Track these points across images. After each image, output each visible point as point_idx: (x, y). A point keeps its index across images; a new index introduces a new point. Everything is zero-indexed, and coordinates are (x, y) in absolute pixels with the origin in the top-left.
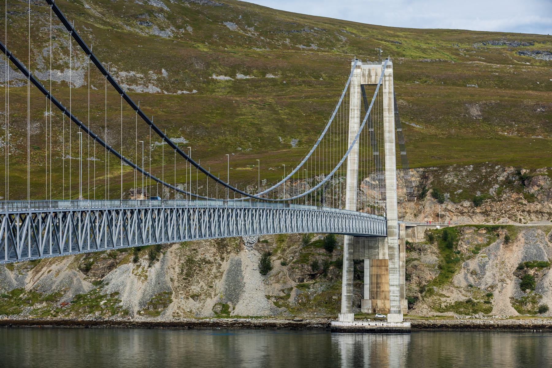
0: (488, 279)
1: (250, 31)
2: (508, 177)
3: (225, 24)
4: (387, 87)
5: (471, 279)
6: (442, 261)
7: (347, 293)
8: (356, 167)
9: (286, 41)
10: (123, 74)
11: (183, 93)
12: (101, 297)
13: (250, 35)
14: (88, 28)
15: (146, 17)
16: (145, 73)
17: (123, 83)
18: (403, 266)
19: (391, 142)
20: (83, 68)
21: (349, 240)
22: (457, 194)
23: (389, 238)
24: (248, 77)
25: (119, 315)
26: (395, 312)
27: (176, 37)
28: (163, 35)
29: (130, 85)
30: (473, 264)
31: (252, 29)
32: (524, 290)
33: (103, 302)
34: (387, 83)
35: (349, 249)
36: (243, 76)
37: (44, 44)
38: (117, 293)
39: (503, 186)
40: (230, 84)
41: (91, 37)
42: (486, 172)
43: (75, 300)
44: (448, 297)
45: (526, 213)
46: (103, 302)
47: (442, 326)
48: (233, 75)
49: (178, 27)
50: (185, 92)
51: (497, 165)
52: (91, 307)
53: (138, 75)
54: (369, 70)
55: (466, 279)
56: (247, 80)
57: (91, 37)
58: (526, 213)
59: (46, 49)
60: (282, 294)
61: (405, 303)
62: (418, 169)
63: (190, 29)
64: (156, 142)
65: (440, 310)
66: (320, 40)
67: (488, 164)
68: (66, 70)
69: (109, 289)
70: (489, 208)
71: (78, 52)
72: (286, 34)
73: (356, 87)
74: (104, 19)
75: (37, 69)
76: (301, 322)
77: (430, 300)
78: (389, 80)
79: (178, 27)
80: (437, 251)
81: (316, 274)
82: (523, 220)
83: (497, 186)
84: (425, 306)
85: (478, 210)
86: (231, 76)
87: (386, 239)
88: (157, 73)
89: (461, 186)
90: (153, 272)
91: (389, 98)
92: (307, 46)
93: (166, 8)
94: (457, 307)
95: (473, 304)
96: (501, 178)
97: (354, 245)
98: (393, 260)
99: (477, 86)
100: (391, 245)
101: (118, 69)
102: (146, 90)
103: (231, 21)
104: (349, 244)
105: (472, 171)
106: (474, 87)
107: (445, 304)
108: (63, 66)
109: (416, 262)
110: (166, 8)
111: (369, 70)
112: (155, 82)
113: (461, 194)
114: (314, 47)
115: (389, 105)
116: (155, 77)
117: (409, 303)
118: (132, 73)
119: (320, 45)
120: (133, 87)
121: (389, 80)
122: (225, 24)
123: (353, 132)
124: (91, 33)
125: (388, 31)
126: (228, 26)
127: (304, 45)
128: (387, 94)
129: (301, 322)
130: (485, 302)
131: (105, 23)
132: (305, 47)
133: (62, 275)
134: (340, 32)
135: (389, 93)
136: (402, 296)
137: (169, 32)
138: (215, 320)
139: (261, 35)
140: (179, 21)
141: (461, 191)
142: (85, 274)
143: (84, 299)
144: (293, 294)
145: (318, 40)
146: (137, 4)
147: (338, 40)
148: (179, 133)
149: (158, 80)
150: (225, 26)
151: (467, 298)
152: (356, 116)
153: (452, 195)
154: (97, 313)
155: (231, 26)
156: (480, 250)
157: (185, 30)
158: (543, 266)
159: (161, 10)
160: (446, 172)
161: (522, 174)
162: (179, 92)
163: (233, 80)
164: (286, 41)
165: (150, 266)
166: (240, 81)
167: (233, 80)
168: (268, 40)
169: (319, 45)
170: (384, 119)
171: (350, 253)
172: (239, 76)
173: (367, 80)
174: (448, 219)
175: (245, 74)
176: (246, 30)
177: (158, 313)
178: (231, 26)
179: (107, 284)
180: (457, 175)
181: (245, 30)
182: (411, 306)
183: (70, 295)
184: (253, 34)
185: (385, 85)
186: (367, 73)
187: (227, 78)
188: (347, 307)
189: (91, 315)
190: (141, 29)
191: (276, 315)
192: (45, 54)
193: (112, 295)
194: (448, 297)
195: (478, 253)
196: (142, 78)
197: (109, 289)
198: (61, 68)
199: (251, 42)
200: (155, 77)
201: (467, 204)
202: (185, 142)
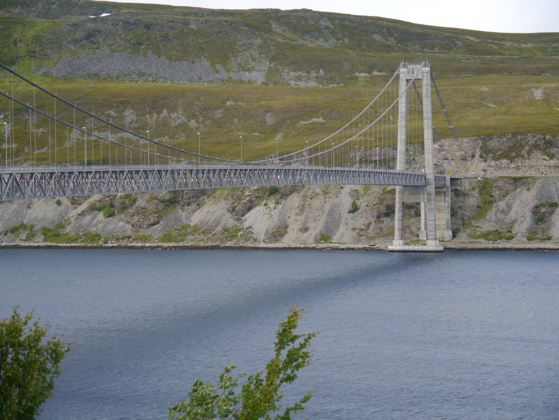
0: (512, 215)
1: (390, 40)
2: (536, 141)
3: (373, 35)
4: (425, 80)
5: (500, 216)
6: (480, 202)
7: (399, 226)
8: (404, 137)
9: (416, 46)
10: (292, 74)
11: (333, 87)
12: (240, 230)
13: (390, 43)
14: (271, 42)
15: (316, 34)
16: (309, 73)
17: (291, 80)
18: (448, 207)
19: (428, 119)
20: (265, 71)
21: (400, 189)
22: (498, 155)
23: (427, 187)
24: (381, 74)
25: (250, 242)
26: (432, 239)
27: (335, 47)
28: (326, 45)
29: (296, 82)
30: (502, 205)
31: (392, 39)
32: (537, 223)
33: (241, 233)
34: (425, 78)
35: (399, 195)
36: (377, 73)
37: (239, 54)
38: (250, 227)
39: (532, 148)
40: (368, 79)
41: (272, 48)
42: (521, 139)
43: (222, 232)
44: (482, 228)
45: (546, 167)
46: (241, 233)
47: (273, 248)
48: (370, 72)
49: (338, 40)
50: (334, 85)
51: (529, 133)
52: (232, 237)
53: (303, 74)
54: (413, 69)
55: (496, 215)
56: (380, 76)
57: (272, 48)
58: (546, 167)
59: (240, 57)
60: (363, 227)
61: (450, 233)
62: (471, 138)
63: (346, 40)
64: (302, 122)
65: (473, 237)
66: (442, 45)
67: (523, 132)
68: (252, 71)
69: (246, 224)
70: (520, 164)
71: (262, 59)
72: (417, 42)
73: (404, 82)
74: (285, 35)
75: (233, 72)
76: (373, 247)
77: (468, 231)
78: (427, 76)
79: (338, 40)
80: (477, 195)
81: (389, 213)
82: (544, 172)
83: (527, 148)
84: (464, 235)
85: (512, 165)
86: (369, 73)
87: (425, 188)
88: (316, 73)
89: (501, 149)
90: (276, 213)
91: (427, 89)
92: (431, 49)
93: (331, 26)
94: (486, 236)
95: (500, 233)
96: (531, 142)
97: (402, 192)
98: (430, 203)
99: (550, 75)
100: (429, 192)
101: (289, 70)
102: (307, 85)
103: (378, 33)
104: (400, 192)
105: (510, 138)
106: (548, 75)
107: (479, 232)
108: (251, 69)
109: (461, 204)
110: (331, 26)
111: (413, 69)
112: (314, 79)
113: (500, 155)
114: (436, 50)
115: (427, 93)
116: (314, 75)
117: (453, 233)
118: (299, 73)
119: (441, 48)
120: (298, 83)
121: (427, 76)
122: (373, 35)
123: (402, 113)
124: (273, 45)
125: (467, 37)
126: (375, 37)
127: (429, 49)
128: (425, 86)
129: (373, 247)
130: (508, 232)
131: (285, 38)
132: (429, 51)
133: (216, 215)
134: (458, 39)
135: (427, 85)
136: (448, 228)
137: (330, 42)
138: (314, 245)
139: (398, 43)
140: (339, 35)
141: (501, 152)
142: (231, 214)
143: (228, 231)
144: (372, 227)
145: (440, 45)
146: (310, 23)
147: (456, 45)
148: (320, 114)
149: (317, 77)
150: (373, 37)
151: (495, 229)
152: (403, 101)
153: (494, 155)
154: (235, 241)
155: (376, 37)
156: (508, 194)
157: (343, 41)
158: (554, 205)
159: (327, 28)
160: (491, 139)
161: (546, 139)
162: (331, 85)
163: (370, 76)
164: (416, 46)
165: (274, 208)
166: (376, 77)
167: (370, 76)
168: (403, 46)
169: (439, 49)
170: (423, 103)
171: (400, 198)
172: (375, 73)
173: (411, 76)
174: (489, 172)
175: (380, 71)
176: (388, 40)
177: (277, 241)
178: (376, 37)
179: (245, 221)
180: (498, 141)
181: (387, 40)
182: (454, 235)
183: (219, 229)
184: (392, 43)
185: (424, 79)
186: (411, 71)
187: (366, 75)
188: (399, 236)
189: (231, 242)
190: (311, 41)
191: (358, 241)
192: (239, 61)
193: (247, 229)
194: (482, 228)
195: (506, 196)
196: (305, 77)
197: (246, 224)
198: (248, 70)
199: (390, 48)
200: (314, 75)
201: (504, 161)
202: (322, 122)
